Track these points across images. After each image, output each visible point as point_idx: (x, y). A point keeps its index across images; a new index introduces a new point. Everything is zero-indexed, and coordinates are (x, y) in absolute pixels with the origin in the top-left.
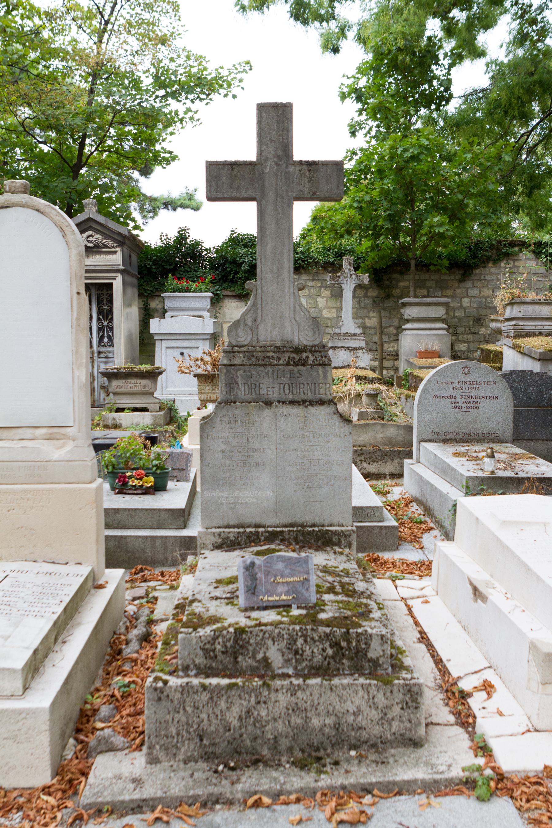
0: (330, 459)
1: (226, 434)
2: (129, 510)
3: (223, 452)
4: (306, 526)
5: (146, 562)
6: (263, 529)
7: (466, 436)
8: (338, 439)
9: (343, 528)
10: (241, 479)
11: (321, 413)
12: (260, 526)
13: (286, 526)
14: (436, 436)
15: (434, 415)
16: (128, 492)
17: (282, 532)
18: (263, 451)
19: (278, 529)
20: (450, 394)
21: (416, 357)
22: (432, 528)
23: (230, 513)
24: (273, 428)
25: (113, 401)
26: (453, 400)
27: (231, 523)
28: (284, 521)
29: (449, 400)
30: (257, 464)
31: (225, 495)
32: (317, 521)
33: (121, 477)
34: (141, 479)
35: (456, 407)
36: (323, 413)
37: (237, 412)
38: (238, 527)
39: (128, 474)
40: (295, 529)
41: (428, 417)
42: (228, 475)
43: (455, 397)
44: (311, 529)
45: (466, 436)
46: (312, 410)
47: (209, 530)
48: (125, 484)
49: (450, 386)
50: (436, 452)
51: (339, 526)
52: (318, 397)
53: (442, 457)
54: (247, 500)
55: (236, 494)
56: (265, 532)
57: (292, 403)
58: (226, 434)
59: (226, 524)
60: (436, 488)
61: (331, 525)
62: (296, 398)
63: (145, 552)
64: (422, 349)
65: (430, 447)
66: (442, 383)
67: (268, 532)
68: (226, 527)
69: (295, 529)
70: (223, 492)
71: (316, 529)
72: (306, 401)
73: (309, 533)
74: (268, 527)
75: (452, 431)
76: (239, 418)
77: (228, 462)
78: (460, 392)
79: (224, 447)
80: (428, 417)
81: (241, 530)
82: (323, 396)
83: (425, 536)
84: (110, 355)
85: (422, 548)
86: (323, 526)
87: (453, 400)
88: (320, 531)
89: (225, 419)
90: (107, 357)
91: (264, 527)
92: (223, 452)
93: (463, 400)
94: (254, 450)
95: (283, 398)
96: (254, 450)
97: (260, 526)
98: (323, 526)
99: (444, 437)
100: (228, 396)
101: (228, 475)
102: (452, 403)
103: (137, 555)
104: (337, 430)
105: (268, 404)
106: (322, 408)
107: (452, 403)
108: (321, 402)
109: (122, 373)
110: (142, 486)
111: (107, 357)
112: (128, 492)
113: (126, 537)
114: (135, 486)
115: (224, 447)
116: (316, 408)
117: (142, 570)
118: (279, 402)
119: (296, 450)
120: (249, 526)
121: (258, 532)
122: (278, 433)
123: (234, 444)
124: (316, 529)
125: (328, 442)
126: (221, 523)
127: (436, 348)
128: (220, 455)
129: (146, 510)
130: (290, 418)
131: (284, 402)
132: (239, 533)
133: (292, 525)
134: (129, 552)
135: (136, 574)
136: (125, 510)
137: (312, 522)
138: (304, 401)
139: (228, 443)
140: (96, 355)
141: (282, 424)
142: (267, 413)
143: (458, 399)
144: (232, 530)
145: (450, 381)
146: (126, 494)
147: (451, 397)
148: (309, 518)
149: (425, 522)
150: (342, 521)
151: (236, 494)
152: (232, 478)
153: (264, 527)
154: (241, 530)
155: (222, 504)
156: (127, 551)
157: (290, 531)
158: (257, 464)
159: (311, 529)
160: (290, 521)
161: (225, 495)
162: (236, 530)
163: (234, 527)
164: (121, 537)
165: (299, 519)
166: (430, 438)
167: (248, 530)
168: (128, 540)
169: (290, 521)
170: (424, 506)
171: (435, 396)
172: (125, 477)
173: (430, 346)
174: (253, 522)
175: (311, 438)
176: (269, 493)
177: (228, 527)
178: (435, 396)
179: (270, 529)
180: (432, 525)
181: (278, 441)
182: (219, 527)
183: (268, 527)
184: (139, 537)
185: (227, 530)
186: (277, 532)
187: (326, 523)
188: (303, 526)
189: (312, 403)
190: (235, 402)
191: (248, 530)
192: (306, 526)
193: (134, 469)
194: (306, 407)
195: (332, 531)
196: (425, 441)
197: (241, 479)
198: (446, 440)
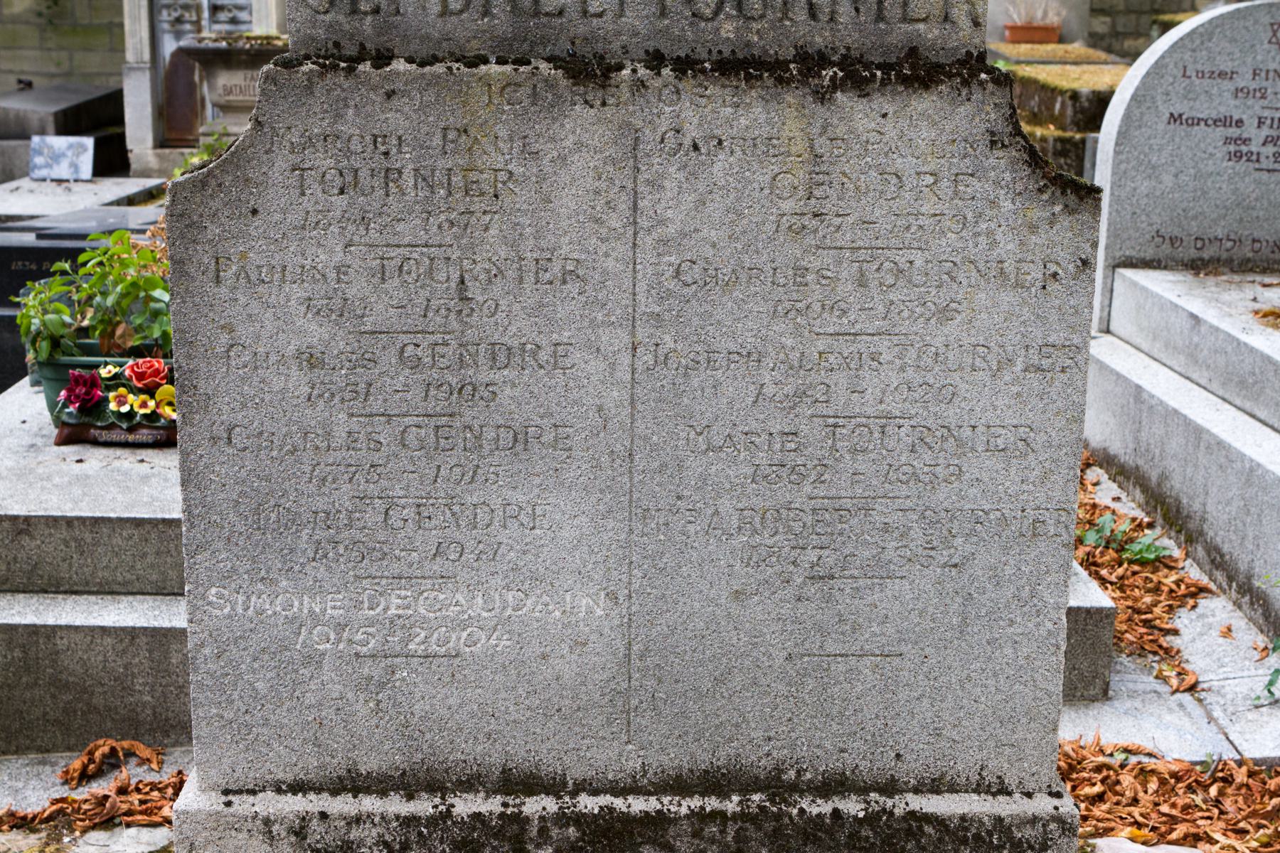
0: (951, 415)
1: (328, 256)
2: (69, 522)
3: (312, 360)
4: (794, 788)
5: (132, 726)
6: (549, 804)
7: (1266, 251)
8: (1007, 298)
9: (1005, 807)
10: (421, 519)
11: (914, 136)
12: (531, 784)
13: (679, 785)
14: (1166, 249)
15: (1168, 180)
16: (105, 436)
17: (659, 820)
18: (557, 361)
19: (638, 805)
20: (1223, 110)
21: (1003, 39)
22: (1202, 590)
23: (363, 710)
24: (615, 222)
25: (219, 129)
26: (1233, 132)
27: (370, 764)
28: (674, 757)
29: (1220, 131)
30: (520, 439)
31: (333, 606)
32: (860, 758)
33: (78, 380)
34: (150, 391)
35: (1238, 156)
36: (927, 132)
37: (396, 119)
38: (407, 785)
39: (104, 372)
40: (732, 805)
41: (1144, 187)
42: (344, 495)
43: (1239, 123)
44: (822, 807)
45: (1266, 251)
46: (860, 115)
47: (243, 805)
48: (92, 407)
49: (1228, 85)
50: (1195, 305)
51: (981, 788)
52: (900, 33)
53: (1226, 325)
54: (458, 640)
55: (394, 604)
56: (562, 819)
57: (739, 68)
58: (328, 256)
59: (336, 765)
60: (1220, 444)
61: (935, 786)
62: (762, 38)
63: (130, 690)
64: (1018, 19)
65: (1163, 285)
66: (1201, 74)
67: (579, 819)
68: (337, 788)
69: (732, 805)
70: (318, 589)
71: (852, 806)
72: (822, 60)
73: (813, 828)
74: (583, 786)
75: (1220, 233)
76: (406, 160)
77: (342, 424)
78: (1257, 107)
79: (315, 332)
80: (1144, 187)
81: (424, 806)
82: (930, 33)
83: (1184, 620)
84: (243, 16)
85: (1192, 688)
86: (891, 788)
87: (1233, 132)
88: (871, 819)
89: (323, 161)
90: (234, 21)
91: (554, 787)
92: (312, 360)
93: (1265, 131)
94: (501, 355)
95: (682, 34)
96: (501, 355)
97: (531, 784)
98: (891, 788)
99: (1193, 253)
100: (338, 16)
101: (344, 495)
102: (1228, 140)
103: (98, 701)
104: (1007, 246)
105: (589, 70)
106: (925, 103)
107: (1228, 140)
108: (918, 71)
109: (242, 51)
110: (153, 417)
111: (234, 21)
112: (105, 436)
113: (52, 631)
114: (131, 415)
115: (315, 332)
116: (881, 102)
117: (112, 762)
118: (655, 60)
119: (753, 357)
120: (469, 785)
121: (519, 820)
122: (646, 256)
123: (381, 313)
124: (852, 806)
125: (945, 314)
126: (310, 765)
127: (1053, 19)
128: (298, 381)
129: (138, 523)
130: (721, 165)
131: (684, 66)
132: (409, 821)
133: (713, 783)
134: (66, 686)
135: (85, 777)
136: (53, 521)
137: (833, 764)
138: (811, 62)
139: (339, 310)
140: (206, 14)
141: (672, 203)
142: (583, 128)
143: (1250, 130)
144: (370, 803)
145: (1227, 66)
146: (96, 443)
147: (1225, 122)
148: (817, 744)
149: (1165, 563)
150: (999, 765)
151: (394, 604)
152: (372, 517)
153: (554, 787)
154: (424, 806)
155: (313, 659)
156: (59, 684)
157: (701, 817)
158: (520, 439)
159: (822, 807)
160: (704, 760)
161: (333, 606)
162: (396, 805)
163: (380, 785)
164: (33, 630)
165: (755, 748)
166: (1149, 253)
167: (464, 806)
168: (61, 644)
169: (703, 757)
170: (1145, 489)
171: (1175, 118)
172: (94, 382)
173: (1039, 14)
174: (496, 759)
175: (846, 288)
176: (588, 605)
177: (352, 784)
178: (1175, 118)
179: (589, 803)
180: (1195, 574)
181: (647, 304)
182: (298, 788)
183: (583, 786)
184: (104, 630)
185: (342, 805)
186: (627, 819)
187: (909, 770)
188: (778, 786)
189: (858, 74)
190: (382, 59)
191: (464, 806)
192: (794, 788)
193: (137, 352)
194: (822, 96)
195: (938, 821)
196: (1130, 263)
197: (421, 519)
198: (1203, 262)
